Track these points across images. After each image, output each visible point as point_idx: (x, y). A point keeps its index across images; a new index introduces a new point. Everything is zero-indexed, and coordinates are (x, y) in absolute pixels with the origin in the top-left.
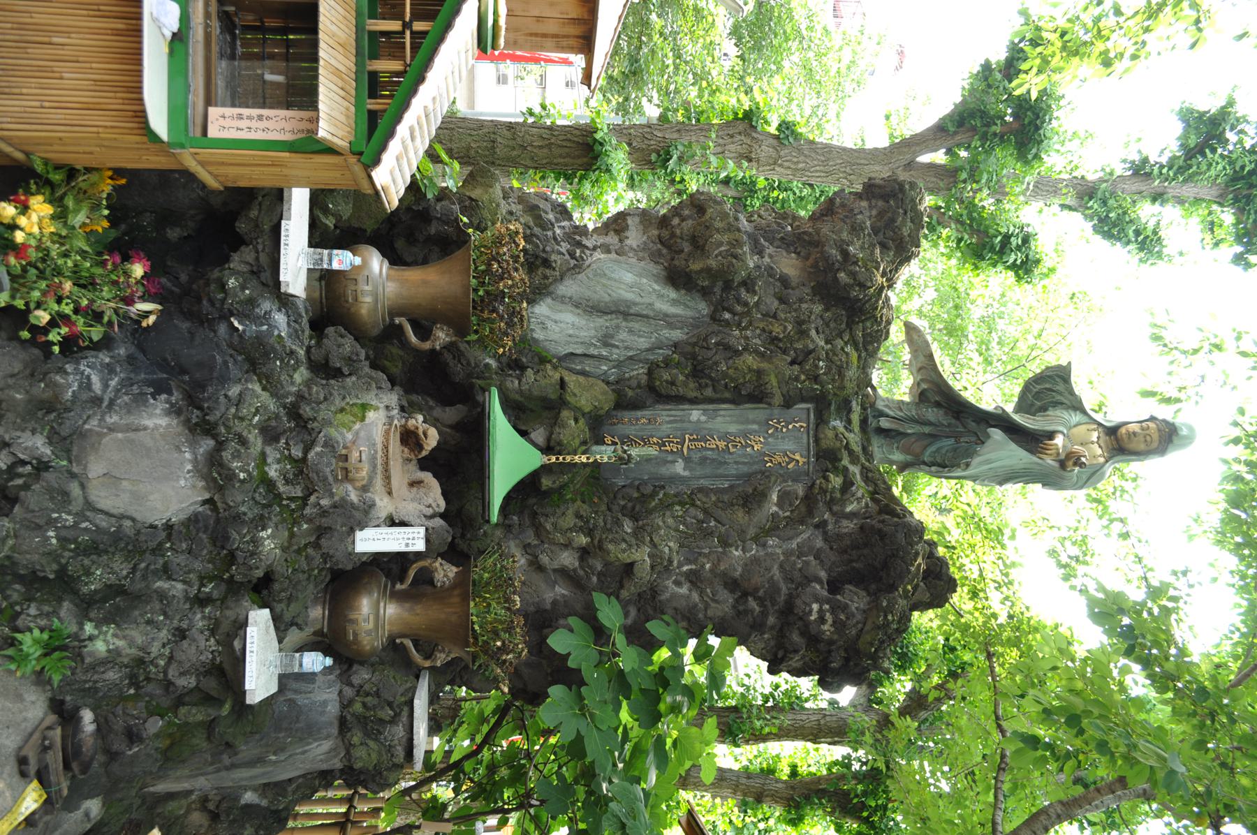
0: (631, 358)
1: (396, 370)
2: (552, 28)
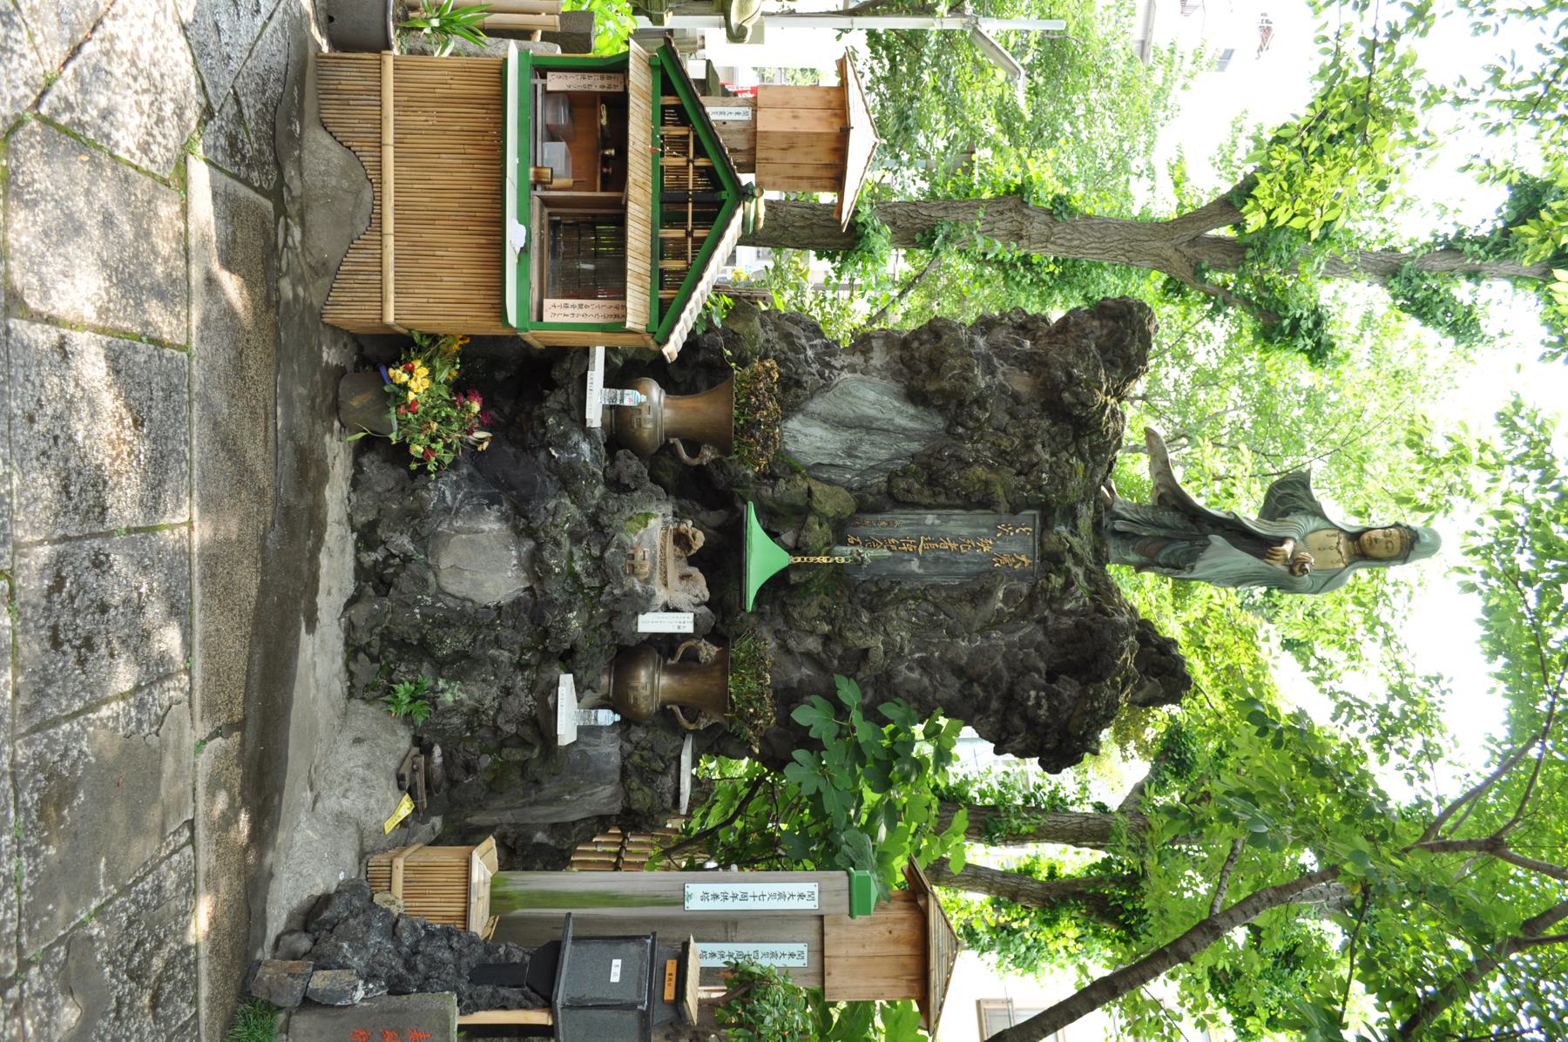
0: (872, 467)
1: (668, 478)
2: (807, 172)
